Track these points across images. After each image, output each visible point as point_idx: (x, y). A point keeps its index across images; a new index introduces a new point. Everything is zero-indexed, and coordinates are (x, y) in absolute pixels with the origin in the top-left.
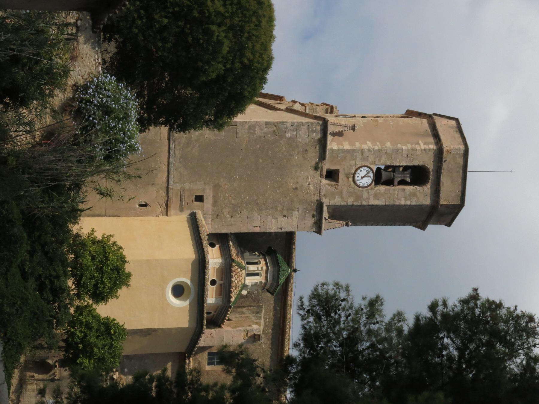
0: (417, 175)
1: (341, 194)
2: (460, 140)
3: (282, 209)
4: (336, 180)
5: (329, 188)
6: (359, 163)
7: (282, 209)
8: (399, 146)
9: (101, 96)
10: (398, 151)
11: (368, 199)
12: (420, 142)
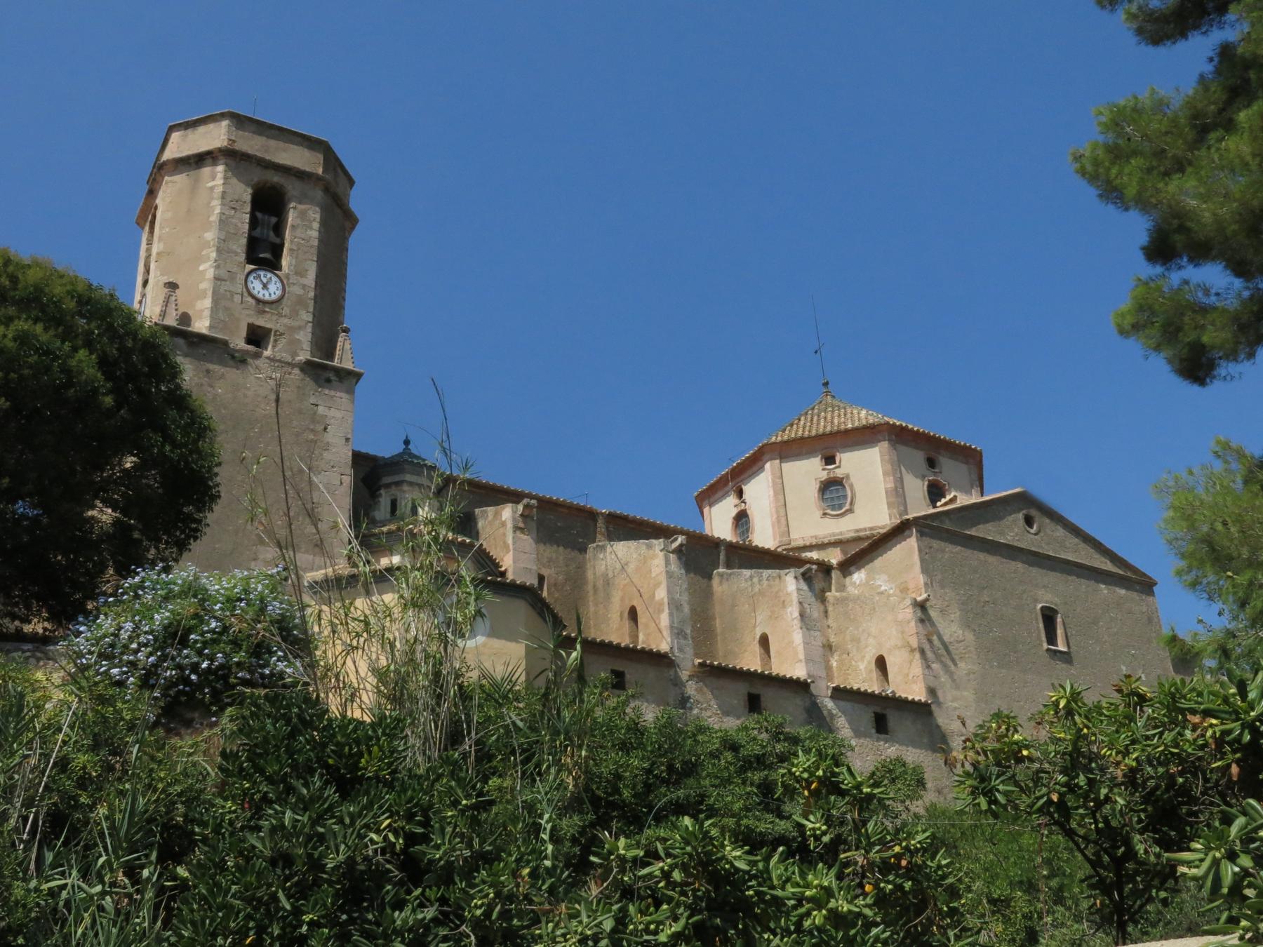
0: (268, 205)
1: (292, 329)
3: (312, 430)
4: (267, 332)
5: (280, 346)
6: (239, 288)
7: (312, 430)
9: (134, 646)
11: (304, 287)
12: (210, 184)
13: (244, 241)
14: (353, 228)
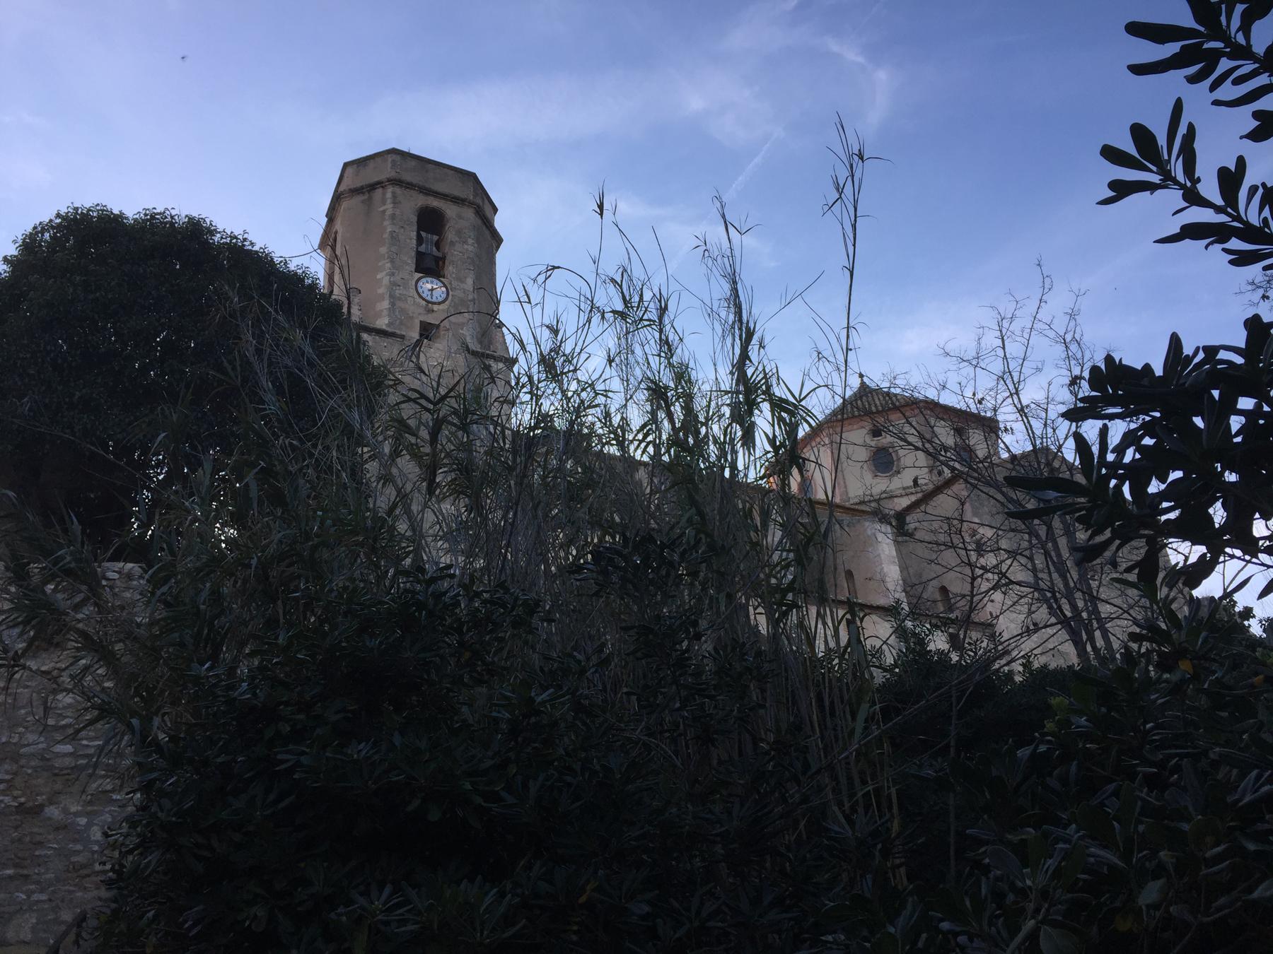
2: (379, 160)
8: (386, 236)
10: (394, 238)
13: (413, 254)
14: (498, 247)
